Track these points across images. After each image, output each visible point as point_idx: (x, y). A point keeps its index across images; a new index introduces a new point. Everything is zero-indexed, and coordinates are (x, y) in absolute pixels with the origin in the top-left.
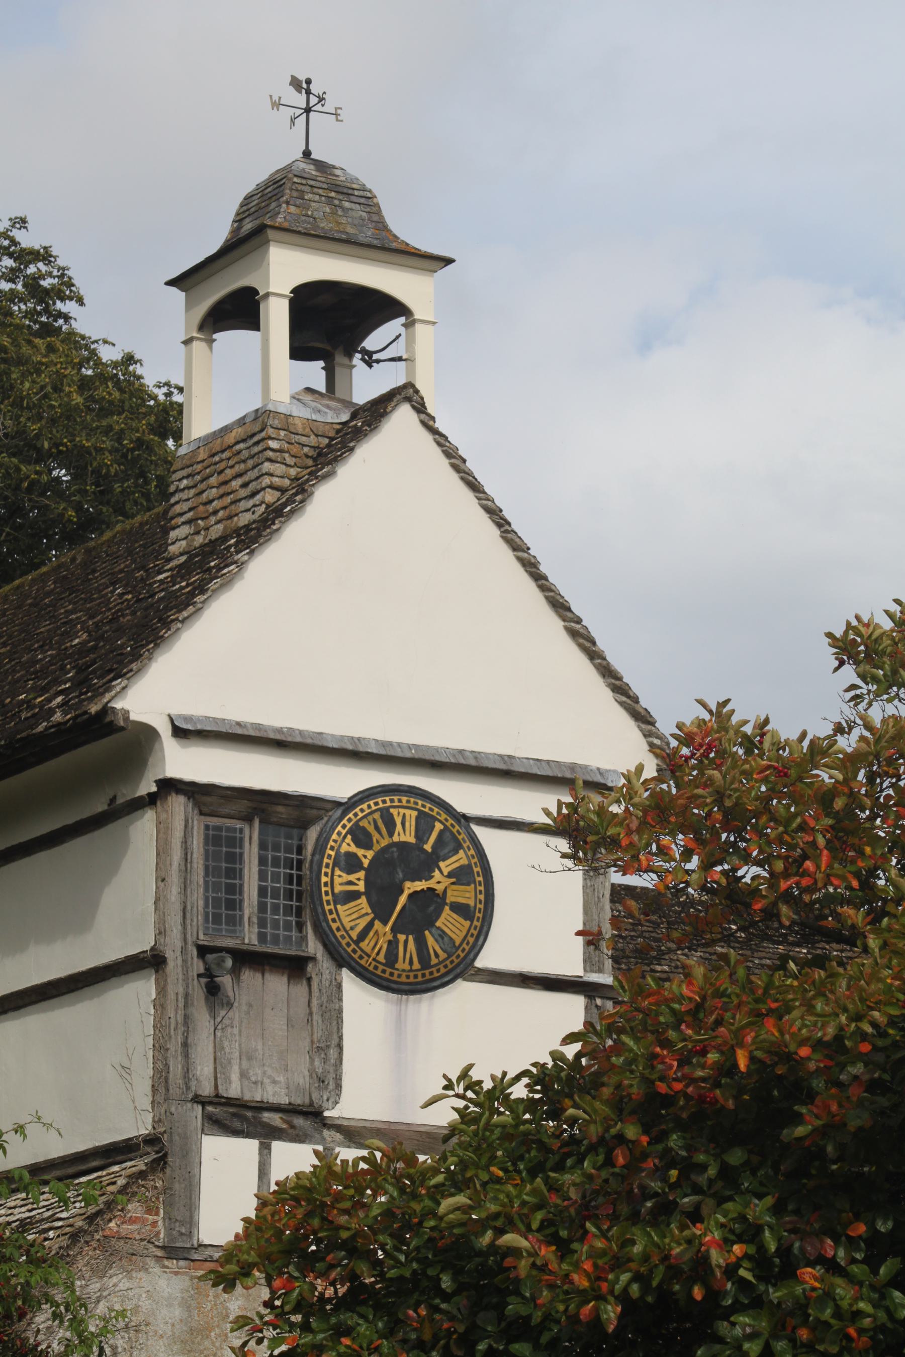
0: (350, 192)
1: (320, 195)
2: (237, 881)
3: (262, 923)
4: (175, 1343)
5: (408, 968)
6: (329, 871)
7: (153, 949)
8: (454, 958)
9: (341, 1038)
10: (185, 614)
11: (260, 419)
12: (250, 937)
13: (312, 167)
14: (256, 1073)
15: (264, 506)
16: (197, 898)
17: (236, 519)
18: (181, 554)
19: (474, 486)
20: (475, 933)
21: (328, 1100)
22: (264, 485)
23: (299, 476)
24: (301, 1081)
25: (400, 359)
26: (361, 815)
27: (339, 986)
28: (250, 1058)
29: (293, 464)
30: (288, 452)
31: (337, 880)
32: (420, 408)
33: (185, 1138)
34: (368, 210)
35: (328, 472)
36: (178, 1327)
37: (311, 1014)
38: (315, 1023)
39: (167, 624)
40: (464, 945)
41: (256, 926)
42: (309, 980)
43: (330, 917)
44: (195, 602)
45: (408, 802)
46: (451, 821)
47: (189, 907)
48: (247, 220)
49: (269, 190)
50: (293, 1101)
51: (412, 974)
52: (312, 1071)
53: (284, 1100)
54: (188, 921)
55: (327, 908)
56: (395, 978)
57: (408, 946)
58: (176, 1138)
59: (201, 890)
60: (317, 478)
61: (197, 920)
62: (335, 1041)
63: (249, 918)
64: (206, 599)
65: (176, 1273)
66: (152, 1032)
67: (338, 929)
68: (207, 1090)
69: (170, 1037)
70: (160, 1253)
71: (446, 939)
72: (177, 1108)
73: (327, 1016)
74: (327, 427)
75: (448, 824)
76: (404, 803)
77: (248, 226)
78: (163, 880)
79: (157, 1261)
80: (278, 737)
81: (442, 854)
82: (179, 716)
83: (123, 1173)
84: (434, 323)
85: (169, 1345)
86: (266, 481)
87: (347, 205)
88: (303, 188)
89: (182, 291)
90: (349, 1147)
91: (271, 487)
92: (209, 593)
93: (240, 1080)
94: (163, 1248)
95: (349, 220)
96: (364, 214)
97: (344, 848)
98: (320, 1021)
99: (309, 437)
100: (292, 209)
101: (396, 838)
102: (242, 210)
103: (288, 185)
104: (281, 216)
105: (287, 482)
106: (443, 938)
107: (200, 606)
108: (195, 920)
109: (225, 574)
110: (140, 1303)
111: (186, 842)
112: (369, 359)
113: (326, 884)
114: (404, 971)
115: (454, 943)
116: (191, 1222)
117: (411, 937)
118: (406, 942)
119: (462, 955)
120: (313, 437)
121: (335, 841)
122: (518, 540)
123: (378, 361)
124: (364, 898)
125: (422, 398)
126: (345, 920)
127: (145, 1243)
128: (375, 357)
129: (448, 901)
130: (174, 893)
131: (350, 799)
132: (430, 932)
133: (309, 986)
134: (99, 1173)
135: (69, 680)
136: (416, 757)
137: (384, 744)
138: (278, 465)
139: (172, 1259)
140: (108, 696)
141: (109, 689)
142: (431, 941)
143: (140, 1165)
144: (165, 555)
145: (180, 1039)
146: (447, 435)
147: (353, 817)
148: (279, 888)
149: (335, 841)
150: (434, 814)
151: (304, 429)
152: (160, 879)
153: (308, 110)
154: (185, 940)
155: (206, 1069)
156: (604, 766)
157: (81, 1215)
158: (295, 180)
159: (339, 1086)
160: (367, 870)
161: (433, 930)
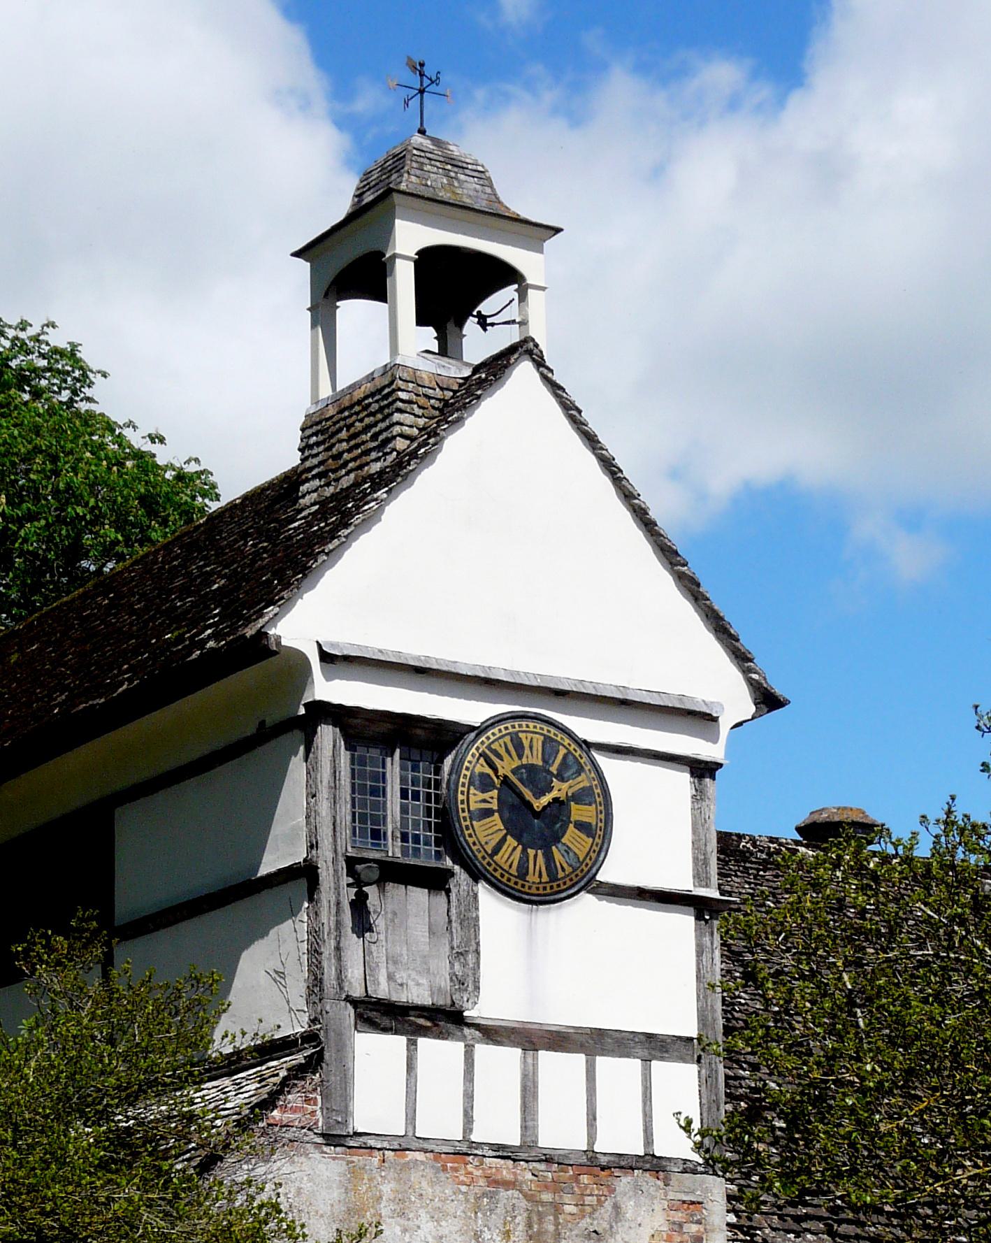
0: (465, 165)
1: (438, 168)
2: (381, 799)
3: (404, 838)
4: (334, 1221)
5: (538, 880)
6: (465, 790)
7: (305, 860)
8: (578, 872)
9: (478, 944)
10: (331, 546)
11: (390, 373)
12: (393, 850)
13: (429, 142)
14: (401, 976)
15: (395, 453)
16: (345, 811)
17: (366, 468)
18: (313, 505)
19: (591, 440)
20: (597, 849)
21: (468, 1001)
22: (395, 433)
23: (428, 425)
24: (443, 984)
25: (513, 322)
26: (493, 738)
27: (476, 896)
28: (395, 963)
29: (421, 414)
30: (416, 403)
31: (472, 798)
32: (540, 363)
33: (340, 1034)
34: (481, 183)
35: (458, 417)
36: (337, 1207)
37: (450, 922)
38: (454, 931)
39: (305, 570)
40: (588, 860)
41: (399, 840)
42: (448, 892)
43: (467, 833)
44: (340, 536)
45: (535, 727)
46: (573, 746)
47: (338, 821)
48: (369, 193)
49: (388, 164)
50: (435, 1002)
51: (541, 886)
52: (453, 977)
53: (428, 1001)
54: (338, 834)
55: (464, 824)
56: (526, 889)
57: (537, 860)
58: (332, 1034)
59: (349, 806)
60: (447, 422)
61: (345, 833)
62: (473, 947)
63: (393, 832)
64: (349, 534)
65: (334, 1159)
66: (306, 937)
67: (474, 844)
68: (358, 992)
69: (324, 941)
70: (319, 1140)
71: (571, 854)
72: (331, 1007)
73: (466, 923)
74: (451, 380)
75: (571, 749)
76: (531, 729)
77: (369, 198)
78: (314, 796)
79: (316, 1148)
80: (417, 664)
81: (566, 775)
82: (327, 643)
83: (284, 1065)
84: (543, 289)
85: (329, 1223)
86: (397, 429)
87: (462, 177)
88: (422, 160)
89: (307, 261)
90: (487, 1044)
91: (402, 436)
92: (352, 528)
93: (388, 982)
94: (323, 1135)
95: (465, 191)
96: (478, 187)
97: (478, 769)
98: (459, 929)
99: (435, 389)
100: (413, 179)
101: (524, 761)
102: (362, 185)
103: (408, 157)
104: (403, 184)
105: (415, 431)
106: (568, 853)
107: (344, 540)
108: (344, 833)
109: (366, 510)
110: (302, 1186)
111: (334, 761)
112: (483, 322)
113: (462, 802)
114: (534, 883)
115: (578, 858)
116: (346, 1112)
117: (539, 851)
118: (536, 856)
119: (586, 869)
120: (438, 389)
121: (469, 762)
122: (629, 487)
123: (492, 324)
124: (496, 814)
125: (541, 352)
126: (481, 835)
127: (305, 1130)
128: (489, 320)
129: (572, 819)
130: (324, 808)
131: (482, 723)
132: (557, 847)
133: (448, 897)
134: (259, 1069)
135: (216, 615)
136: (542, 685)
137: (512, 673)
138: (407, 415)
139: (330, 1145)
140: (261, 622)
141: (261, 615)
142: (557, 856)
143: (299, 1058)
144: (297, 507)
145: (333, 943)
146: (565, 387)
147: (485, 740)
148: (419, 805)
149: (469, 762)
150: (559, 739)
151: (430, 382)
152: (310, 796)
153: (422, 92)
154: (335, 851)
155: (356, 971)
156: (708, 699)
157: (246, 1104)
158: (415, 152)
159: (477, 988)
160: (499, 790)
161: (560, 846)
